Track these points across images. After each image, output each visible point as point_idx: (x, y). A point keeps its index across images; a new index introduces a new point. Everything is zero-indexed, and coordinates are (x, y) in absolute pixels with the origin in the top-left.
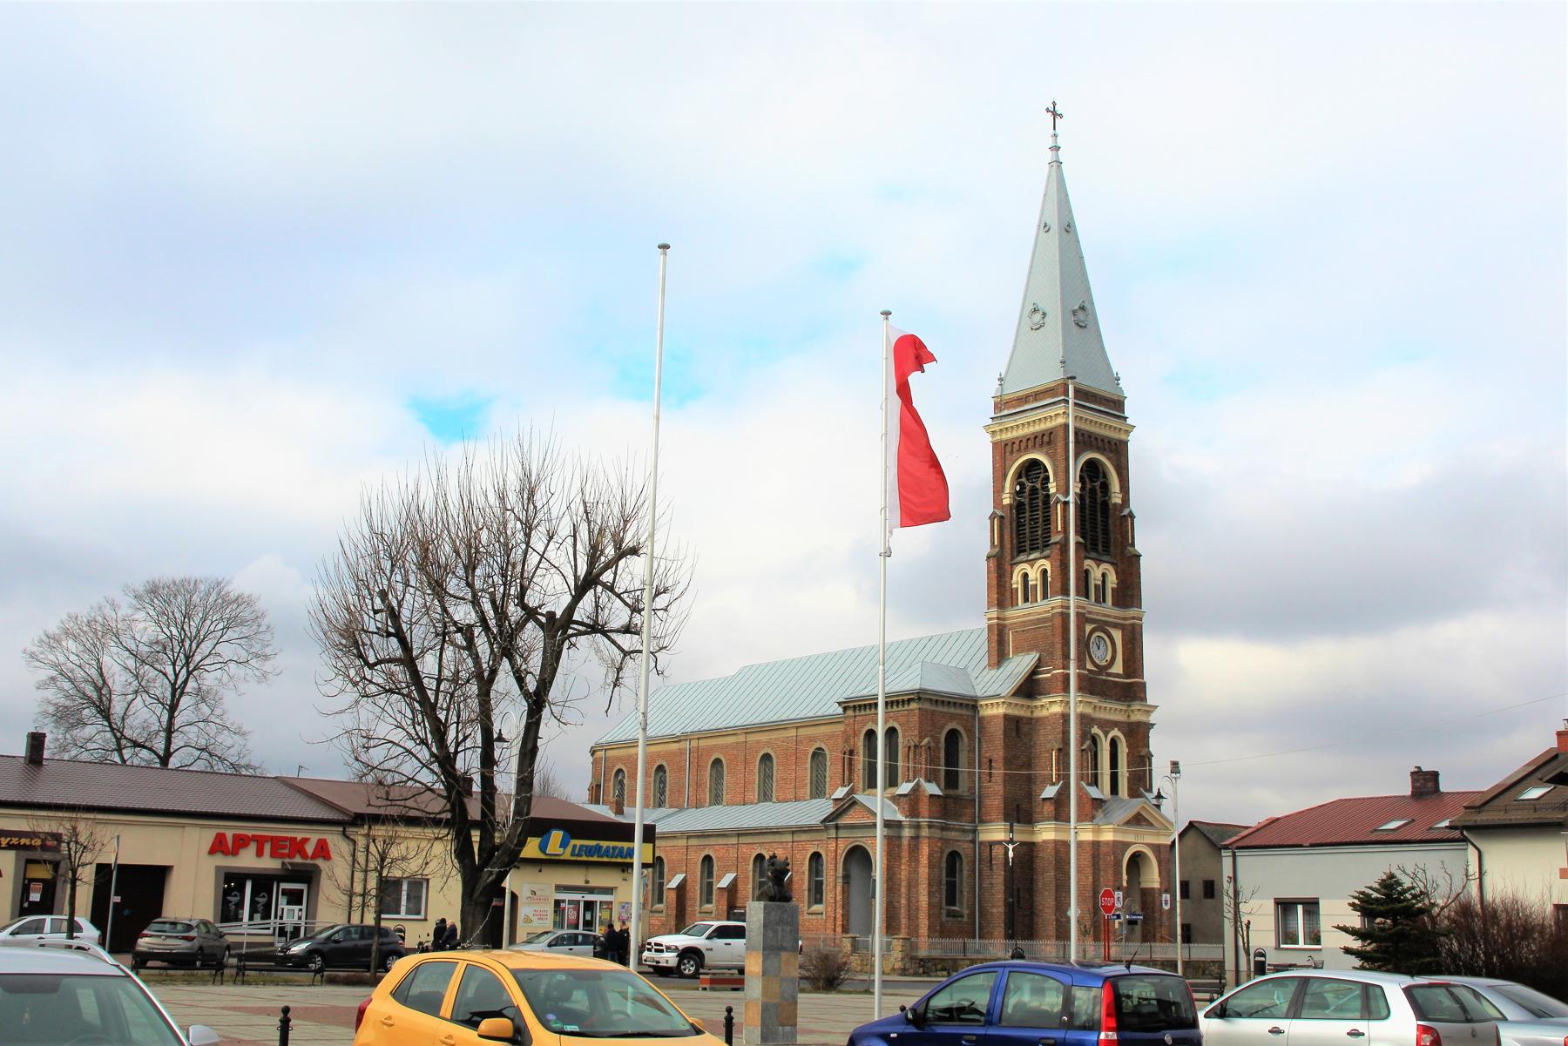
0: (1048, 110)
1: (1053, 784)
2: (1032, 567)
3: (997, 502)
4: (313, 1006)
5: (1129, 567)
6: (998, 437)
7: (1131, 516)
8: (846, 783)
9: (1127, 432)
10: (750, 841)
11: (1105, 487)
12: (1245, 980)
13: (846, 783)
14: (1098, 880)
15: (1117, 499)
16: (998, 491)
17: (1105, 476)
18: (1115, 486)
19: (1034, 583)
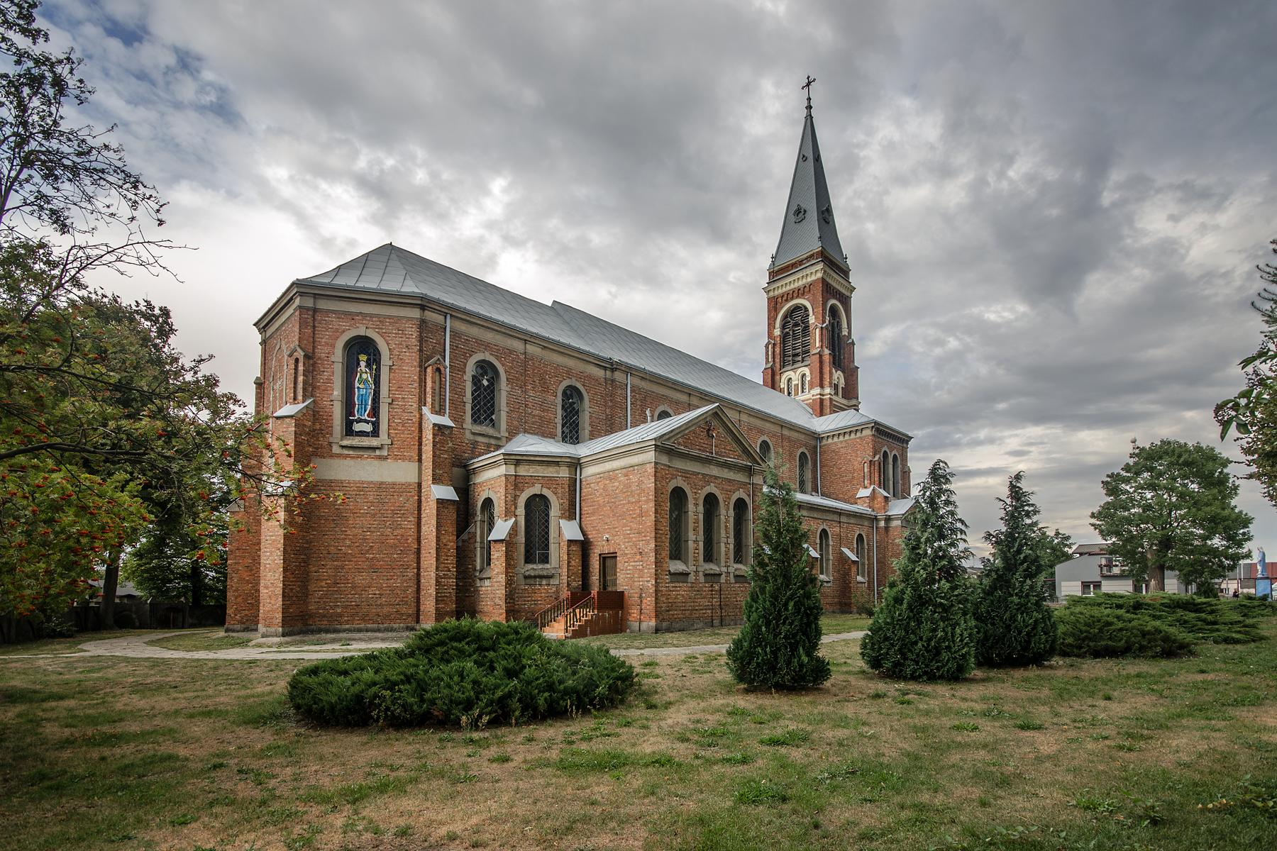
0: (808, 78)
1: (866, 488)
2: (795, 373)
3: (770, 335)
4: (305, 648)
5: (851, 374)
6: (771, 294)
7: (853, 343)
8: (300, 398)
9: (852, 291)
10: (815, 516)
11: (839, 324)
12: (587, 436)
13: (300, 398)
14: (420, 386)
15: (845, 332)
16: (771, 326)
17: (839, 318)
18: (845, 325)
19: (797, 382)
